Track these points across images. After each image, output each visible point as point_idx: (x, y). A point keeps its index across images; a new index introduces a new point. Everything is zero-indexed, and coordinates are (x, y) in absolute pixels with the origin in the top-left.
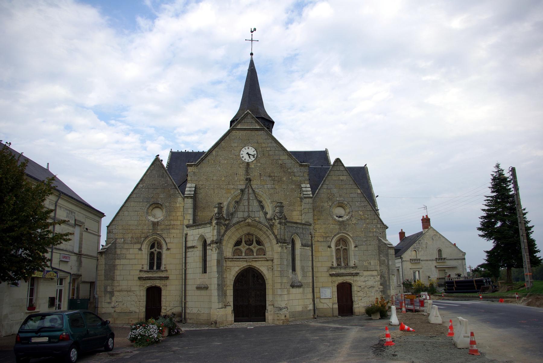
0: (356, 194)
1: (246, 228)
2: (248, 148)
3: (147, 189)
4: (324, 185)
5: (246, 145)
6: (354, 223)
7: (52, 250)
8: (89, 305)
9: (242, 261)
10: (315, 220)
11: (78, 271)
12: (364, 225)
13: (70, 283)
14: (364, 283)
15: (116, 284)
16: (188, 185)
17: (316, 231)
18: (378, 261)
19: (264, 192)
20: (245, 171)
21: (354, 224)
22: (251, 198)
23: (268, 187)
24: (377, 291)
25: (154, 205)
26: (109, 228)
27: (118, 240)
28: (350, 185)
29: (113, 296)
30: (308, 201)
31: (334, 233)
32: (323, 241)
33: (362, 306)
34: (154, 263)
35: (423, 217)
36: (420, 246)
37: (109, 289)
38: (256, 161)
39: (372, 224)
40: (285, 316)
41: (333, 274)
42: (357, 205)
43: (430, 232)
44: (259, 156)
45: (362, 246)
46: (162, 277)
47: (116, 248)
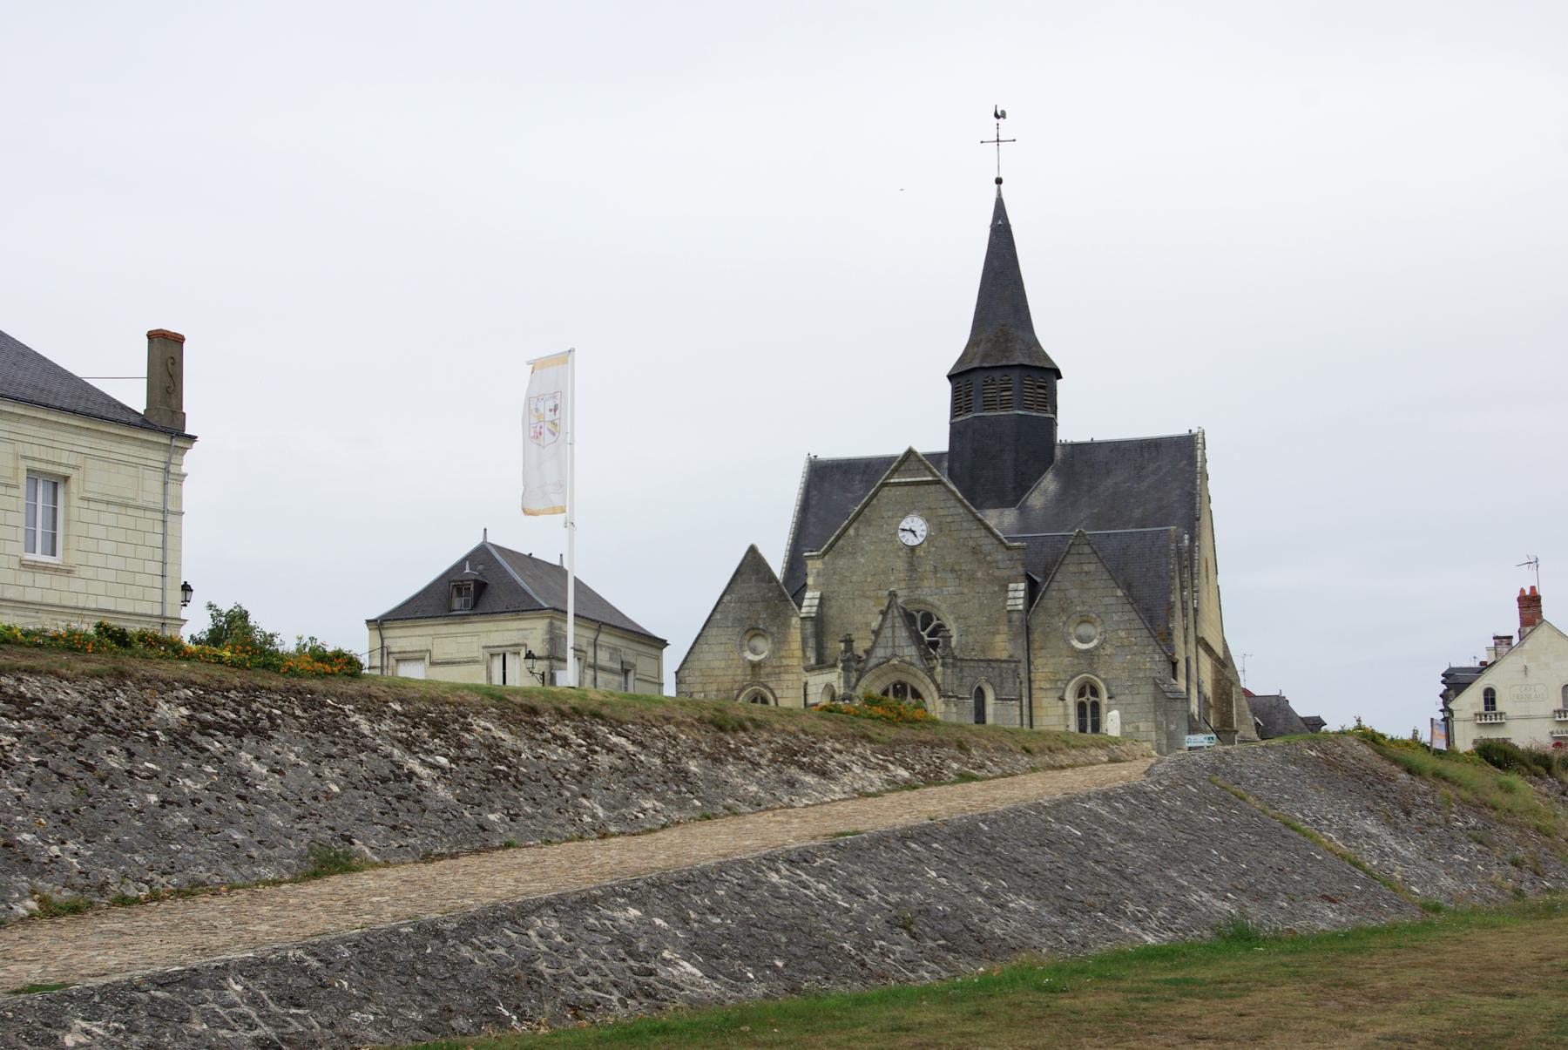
16: (808, 595)
35: (1522, 591)
45: (1123, 697)
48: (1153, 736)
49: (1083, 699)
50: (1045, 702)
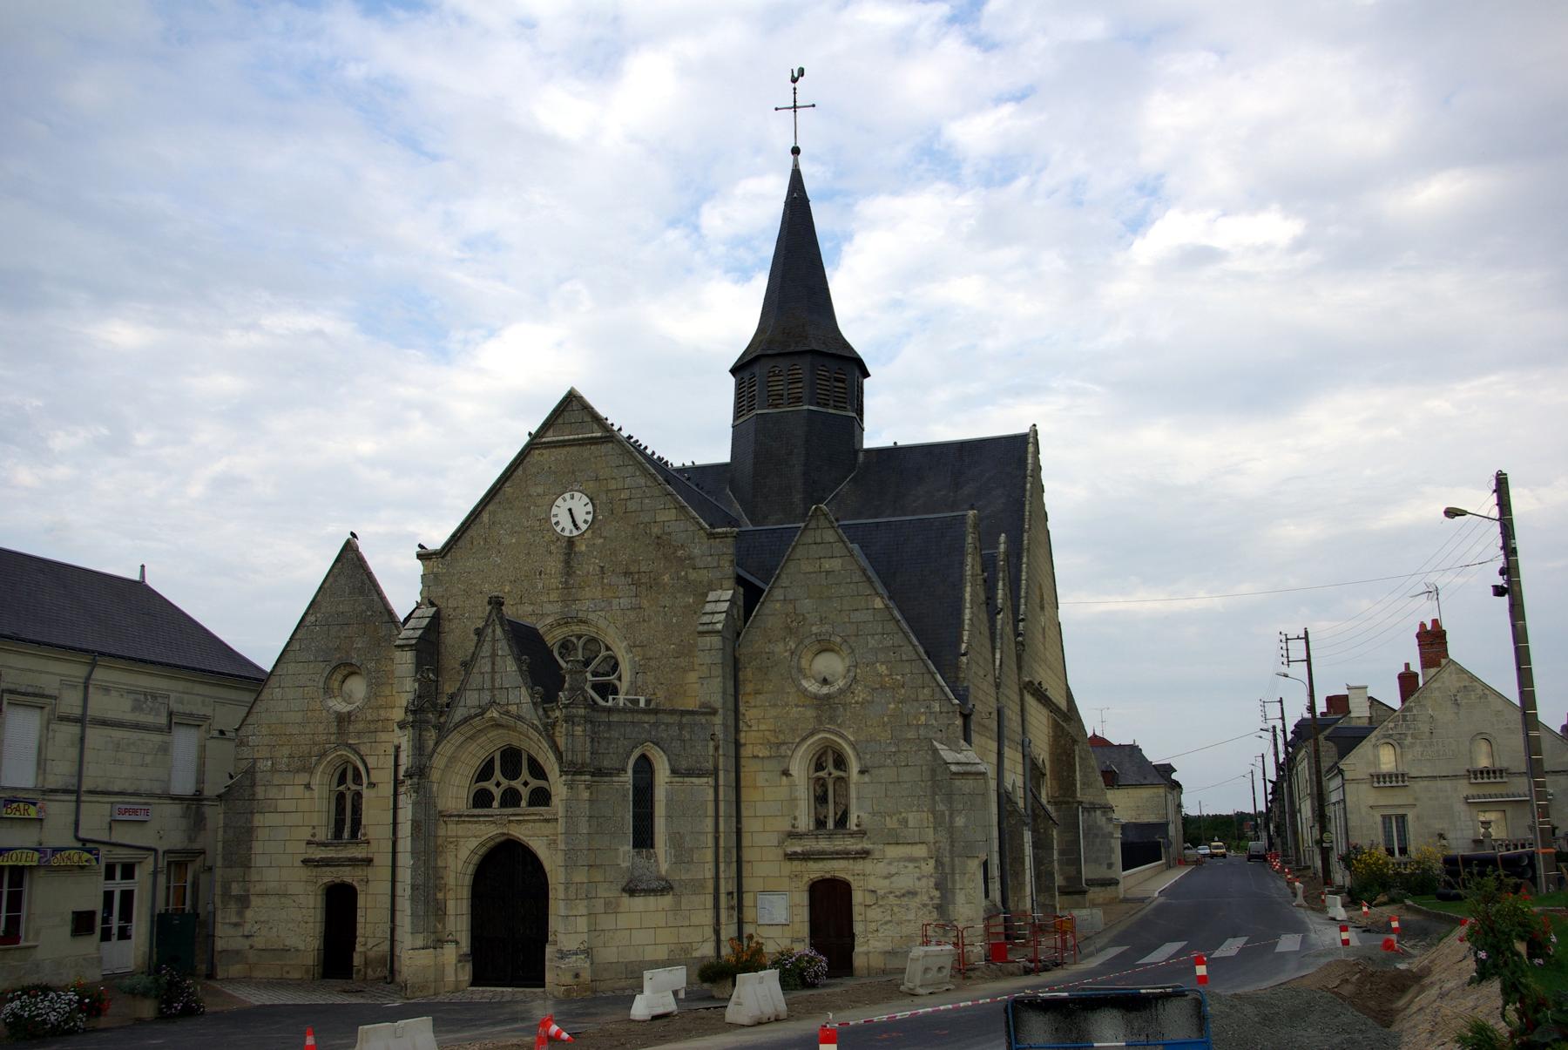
0: (869, 611)
1: (495, 733)
2: (572, 497)
3: (325, 628)
4: (776, 590)
5: (566, 488)
6: (860, 699)
7: (78, 797)
8: (197, 930)
9: (485, 822)
10: (749, 694)
11: (191, 840)
12: (892, 706)
13: (155, 873)
14: (887, 882)
15: (255, 877)
17: (750, 727)
18: (930, 815)
19: (610, 620)
20: (562, 562)
21: (862, 704)
22: (500, 653)
23: (622, 605)
24: (925, 905)
25: (342, 668)
26: (240, 732)
27: (260, 765)
28: (851, 586)
29: (248, 907)
30: (709, 644)
31: (799, 732)
32: (768, 757)
33: (878, 950)
34: (343, 821)
35: (1423, 625)
36: (1408, 728)
37: (236, 889)
38: (592, 533)
39: (915, 704)
40: (577, 976)
41: (795, 853)
42: (870, 646)
43: (1448, 679)
44: (601, 517)
45: (882, 771)
46: (313, 859)
47: (253, 785)
48: (930, 835)
49: (821, 774)
50: (761, 779)
